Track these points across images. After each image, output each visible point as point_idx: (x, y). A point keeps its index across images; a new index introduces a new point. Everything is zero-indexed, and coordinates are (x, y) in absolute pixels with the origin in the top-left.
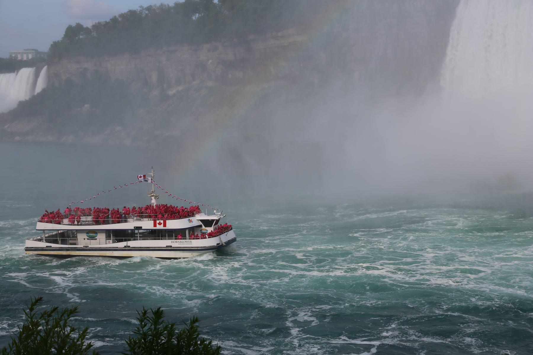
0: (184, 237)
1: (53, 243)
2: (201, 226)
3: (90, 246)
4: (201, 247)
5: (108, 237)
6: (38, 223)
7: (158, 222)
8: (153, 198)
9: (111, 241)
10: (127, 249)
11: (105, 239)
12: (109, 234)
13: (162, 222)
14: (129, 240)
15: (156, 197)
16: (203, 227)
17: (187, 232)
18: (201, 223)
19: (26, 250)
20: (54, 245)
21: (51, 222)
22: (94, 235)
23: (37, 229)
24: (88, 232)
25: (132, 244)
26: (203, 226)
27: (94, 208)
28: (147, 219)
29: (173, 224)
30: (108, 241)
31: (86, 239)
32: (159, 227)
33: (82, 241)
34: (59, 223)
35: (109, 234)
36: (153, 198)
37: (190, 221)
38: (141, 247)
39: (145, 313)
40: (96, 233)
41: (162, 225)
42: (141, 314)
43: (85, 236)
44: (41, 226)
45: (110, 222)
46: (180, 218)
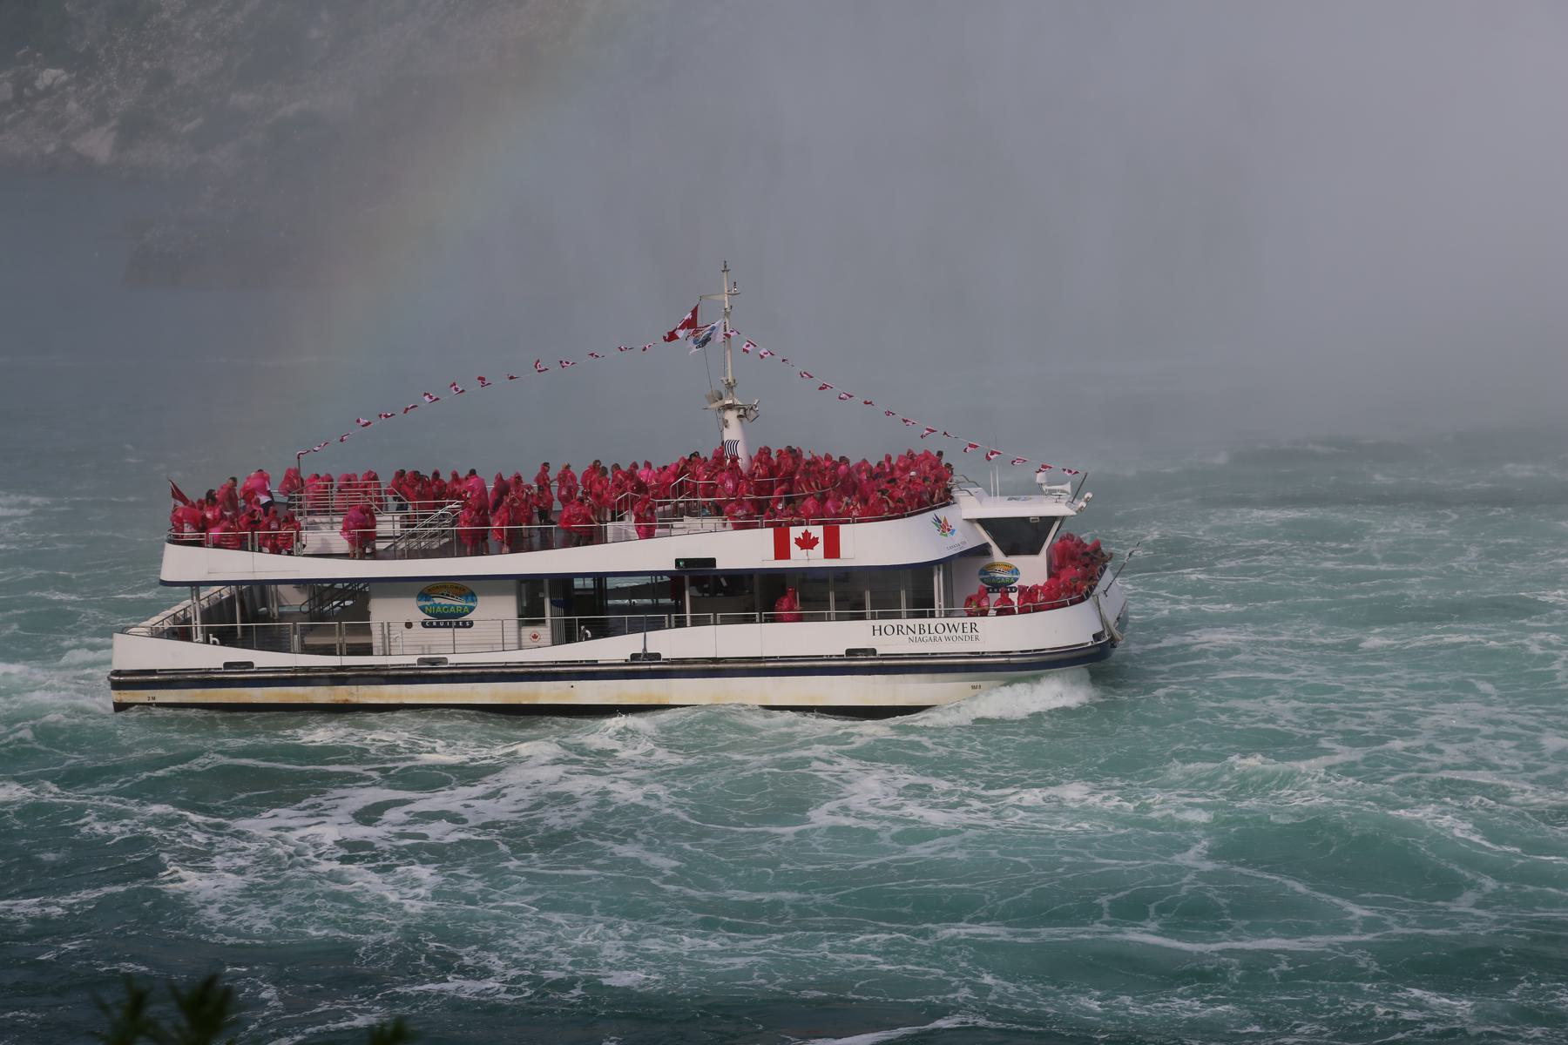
0: (922, 606)
1: (263, 647)
2: (983, 550)
3: (453, 659)
4: (1024, 653)
5: (530, 614)
6: (170, 548)
7: (796, 532)
8: (731, 416)
9: (545, 632)
10: (646, 667)
11: (512, 625)
12: (533, 596)
13: (817, 531)
14: (658, 625)
15: (745, 414)
16: (998, 555)
17: (546, 582)
18: (987, 539)
19: (116, 686)
20: (263, 659)
21: (240, 544)
22: (458, 603)
23: (166, 577)
24: (427, 588)
25: (671, 642)
26: (995, 549)
27: (499, 479)
28: (710, 522)
29: (871, 544)
30: (528, 631)
31: (417, 627)
32: (799, 558)
33: (400, 632)
34: (281, 546)
35: (533, 596)
36: (731, 416)
37: (944, 527)
38: (715, 660)
39: (138, 1001)
40: (472, 595)
41: (819, 548)
42: (118, 1014)
43: (410, 609)
44: (181, 563)
45: (558, 536)
46: (899, 512)
